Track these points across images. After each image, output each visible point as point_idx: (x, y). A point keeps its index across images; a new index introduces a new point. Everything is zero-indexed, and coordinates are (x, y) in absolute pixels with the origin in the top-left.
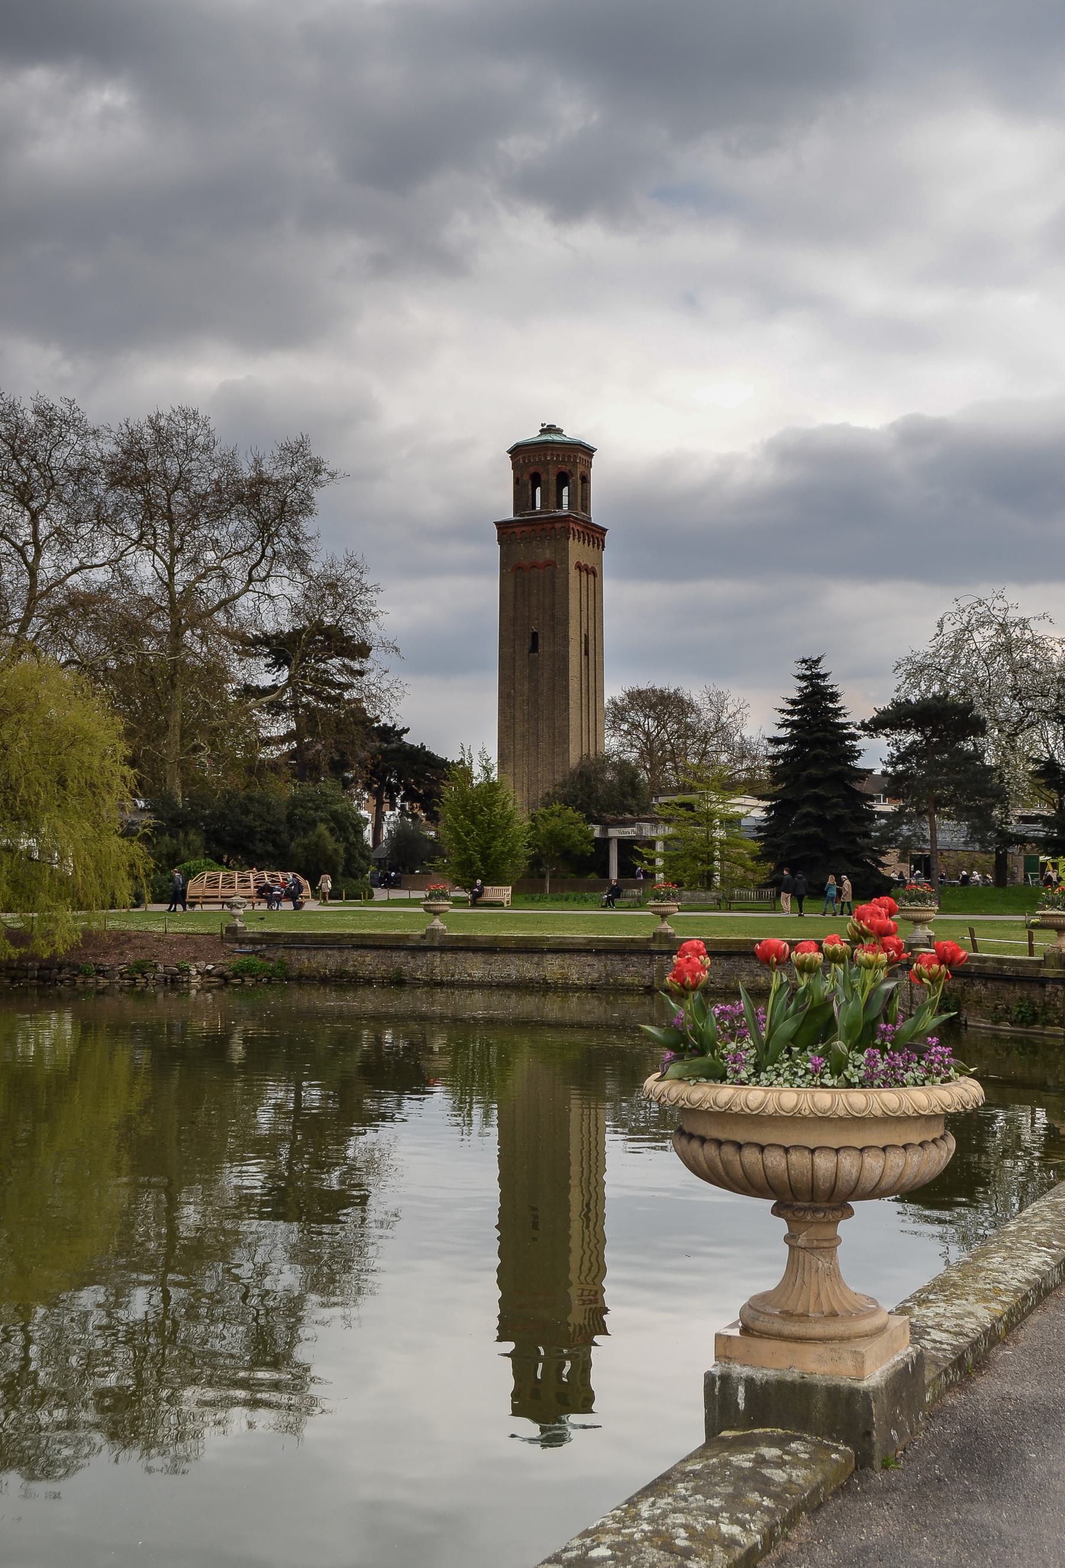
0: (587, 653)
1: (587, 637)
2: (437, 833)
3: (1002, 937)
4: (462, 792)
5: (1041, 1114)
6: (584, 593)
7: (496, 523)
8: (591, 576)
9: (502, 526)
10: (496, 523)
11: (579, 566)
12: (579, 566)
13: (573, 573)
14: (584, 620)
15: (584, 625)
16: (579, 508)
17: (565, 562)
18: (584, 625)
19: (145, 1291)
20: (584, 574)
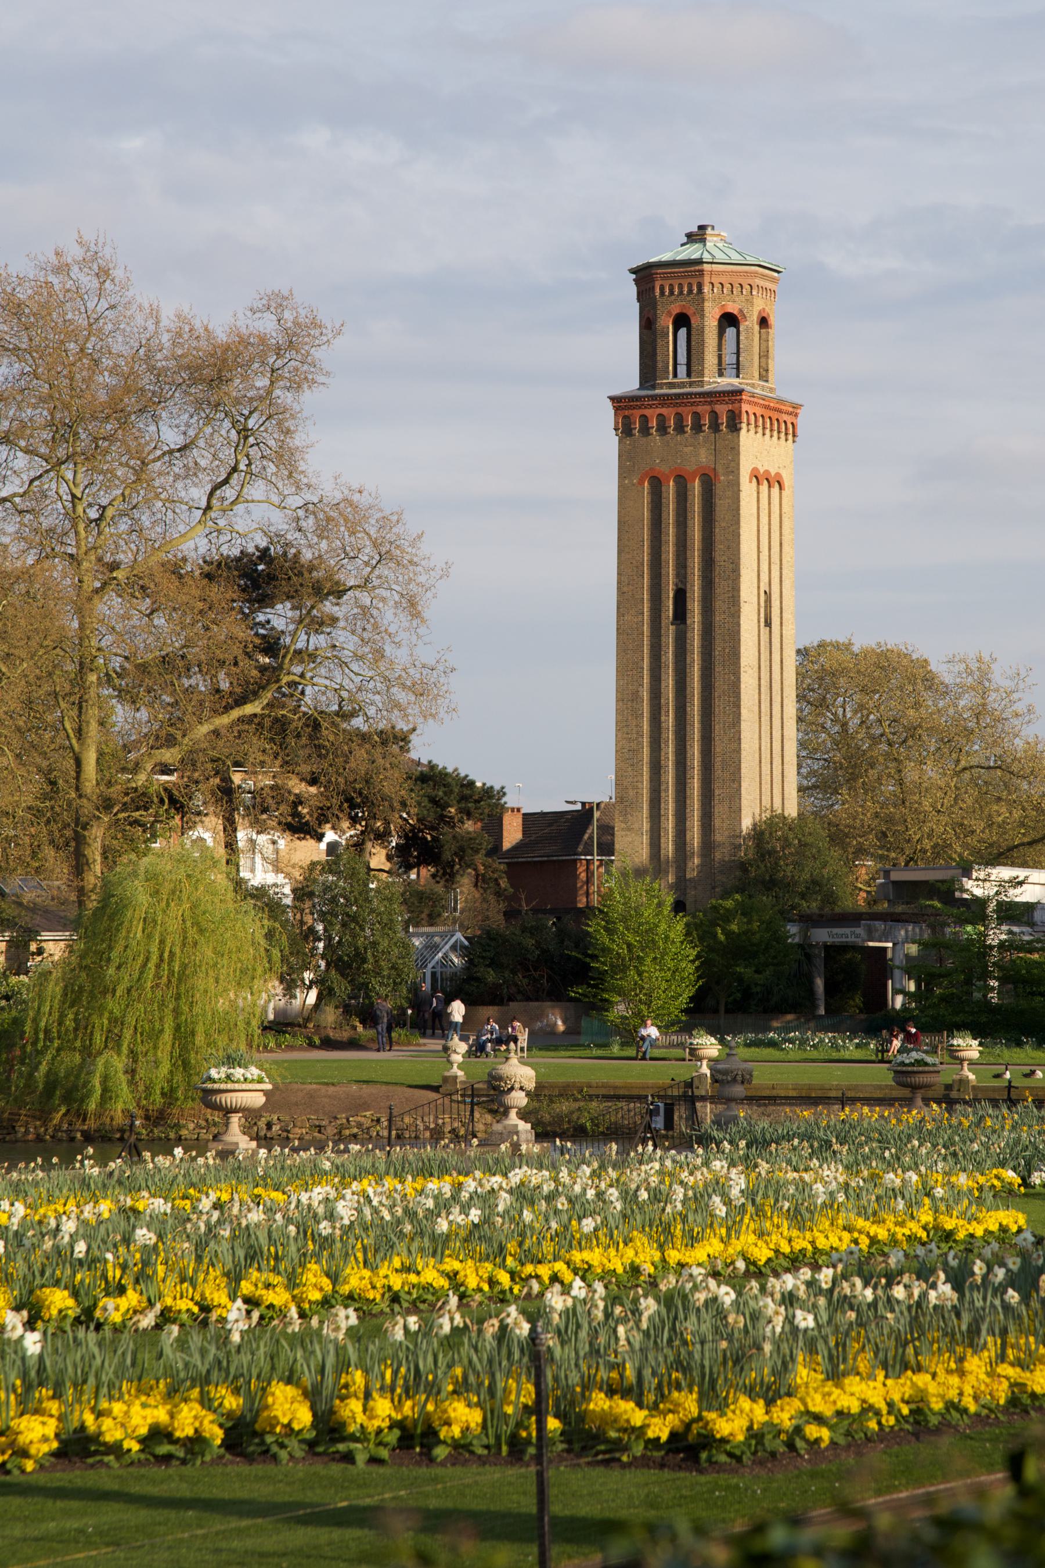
0: (768, 624)
1: (768, 595)
2: (448, 1001)
3: (69, 1208)
4: (270, 1151)
5: (614, 1147)
6: (764, 520)
7: (612, 399)
8: (776, 489)
9: (619, 403)
10: (612, 399)
11: (756, 476)
12: (756, 476)
13: (747, 489)
14: (764, 567)
15: (764, 577)
16: (756, 375)
17: (734, 470)
18: (764, 577)
19: (414, 755)
20: (764, 487)
